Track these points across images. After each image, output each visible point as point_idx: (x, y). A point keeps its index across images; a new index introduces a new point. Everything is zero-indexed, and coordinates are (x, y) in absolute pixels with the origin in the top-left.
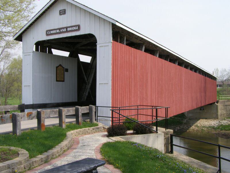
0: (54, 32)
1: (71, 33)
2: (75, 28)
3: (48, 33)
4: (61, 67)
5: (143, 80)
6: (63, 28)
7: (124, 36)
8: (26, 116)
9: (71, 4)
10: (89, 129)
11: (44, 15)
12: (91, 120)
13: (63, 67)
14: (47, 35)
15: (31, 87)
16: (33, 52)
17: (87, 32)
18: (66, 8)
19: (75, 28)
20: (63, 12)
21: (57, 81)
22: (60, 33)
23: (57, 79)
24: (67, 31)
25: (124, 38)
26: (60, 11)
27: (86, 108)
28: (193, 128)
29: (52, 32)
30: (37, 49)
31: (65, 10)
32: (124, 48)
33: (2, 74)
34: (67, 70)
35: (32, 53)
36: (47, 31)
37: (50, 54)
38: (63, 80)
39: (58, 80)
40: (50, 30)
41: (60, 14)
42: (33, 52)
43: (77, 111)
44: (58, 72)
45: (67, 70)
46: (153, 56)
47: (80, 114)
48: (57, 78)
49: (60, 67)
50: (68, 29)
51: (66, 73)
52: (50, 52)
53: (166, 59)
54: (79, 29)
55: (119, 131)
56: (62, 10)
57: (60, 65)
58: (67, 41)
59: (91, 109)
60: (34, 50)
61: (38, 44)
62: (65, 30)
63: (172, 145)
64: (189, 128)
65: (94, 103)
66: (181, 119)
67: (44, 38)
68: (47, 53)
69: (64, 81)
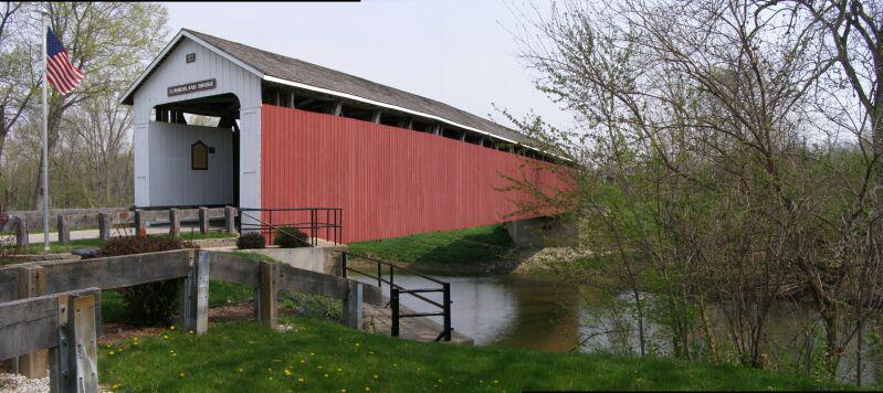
0: (179, 90)
2: (208, 84)
3: (171, 91)
12: (228, 230)
14: (170, 95)
20: (191, 59)
21: (193, 169)
22: (188, 92)
24: (198, 90)
28: (523, 267)
32: (291, 113)
34: (212, 150)
36: (169, 89)
37: (181, 125)
40: (173, 88)
41: (188, 62)
42: (150, 122)
43: (201, 214)
45: (212, 150)
51: (210, 155)
53: (395, 125)
54: (214, 86)
59: (227, 213)
60: (153, 118)
63: (345, 269)
64: (515, 267)
65: (236, 203)
67: (166, 100)
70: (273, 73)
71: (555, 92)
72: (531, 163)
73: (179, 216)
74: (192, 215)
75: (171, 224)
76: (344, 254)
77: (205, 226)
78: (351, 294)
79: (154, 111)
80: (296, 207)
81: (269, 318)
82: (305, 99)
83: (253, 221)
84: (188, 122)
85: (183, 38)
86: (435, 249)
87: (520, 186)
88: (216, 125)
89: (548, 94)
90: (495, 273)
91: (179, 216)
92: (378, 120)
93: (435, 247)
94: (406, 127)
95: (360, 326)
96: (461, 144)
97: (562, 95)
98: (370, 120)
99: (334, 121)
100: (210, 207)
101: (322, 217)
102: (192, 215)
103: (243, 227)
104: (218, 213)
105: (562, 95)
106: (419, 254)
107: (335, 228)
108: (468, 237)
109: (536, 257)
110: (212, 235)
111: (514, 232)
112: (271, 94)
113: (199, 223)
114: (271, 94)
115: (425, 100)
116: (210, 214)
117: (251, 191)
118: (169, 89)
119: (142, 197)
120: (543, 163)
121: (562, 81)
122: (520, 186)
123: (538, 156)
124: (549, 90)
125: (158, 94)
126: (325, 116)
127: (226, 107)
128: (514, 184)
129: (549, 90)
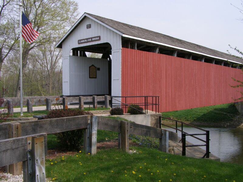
0: (83, 41)
1: (94, 42)
2: (97, 39)
3: (80, 42)
4: (93, 67)
5: (156, 76)
6: (89, 38)
7: (135, 43)
8: (55, 100)
9: (94, 21)
10: (100, 111)
11: (77, 28)
12: (106, 107)
13: (95, 67)
14: (79, 43)
15: (69, 82)
16: (70, 56)
17: (105, 42)
18: (91, 23)
19: (97, 39)
20: (89, 27)
21: (90, 78)
23: (95, 78)
24: (92, 41)
25: (135, 44)
26: (87, 25)
27: (102, 97)
29: (82, 41)
30: (74, 54)
31: (90, 25)
32: (135, 52)
33: (60, 71)
34: (99, 69)
35: (69, 58)
36: (79, 41)
37: (84, 58)
38: (95, 77)
39: (90, 77)
40: (81, 40)
41: (87, 28)
42: (70, 56)
43: (94, 99)
44: (91, 71)
45: (99, 69)
46: (171, 56)
47: (96, 101)
48: (90, 75)
49: (92, 67)
50: (93, 39)
51: (98, 71)
52: (85, 55)
53: (183, 57)
54: (100, 39)
55: (117, 112)
56: (88, 25)
57: (93, 65)
58: (96, 46)
59: (106, 98)
60: (71, 54)
61: (75, 51)
62: (90, 40)
65: (110, 94)
66: (233, 115)
67: (77, 46)
68: (79, 56)
69: (96, 78)
70: (127, 33)
73: (83, 99)
74: (90, 99)
75: (80, 104)
76: (160, 117)
77: (96, 105)
78: (163, 136)
79: (72, 51)
80: (138, 96)
81: (125, 147)
82: (142, 45)
83: (118, 102)
84: (88, 56)
85: (85, 17)
86: (203, 115)
88: (100, 57)
91: (83, 99)
92: (176, 55)
94: (189, 58)
95: (167, 151)
96: (213, 65)
98: (172, 55)
99: (156, 55)
100: (98, 95)
101: (150, 100)
102: (90, 99)
103: (113, 105)
104: (101, 99)
106: (195, 117)
107: (156, 106)
108: (216, 109)
110: (99, 109)
111: (239, 108)
112: (126, 43)
113: (93, 103)
114: (126, 43)
115: (197, 45)
116: (98, 99)
117: (117, 88)
118: (79, 41)
119: (66, 91)
125: (73, 43)
126: (151, 54)
127: (105, 49)
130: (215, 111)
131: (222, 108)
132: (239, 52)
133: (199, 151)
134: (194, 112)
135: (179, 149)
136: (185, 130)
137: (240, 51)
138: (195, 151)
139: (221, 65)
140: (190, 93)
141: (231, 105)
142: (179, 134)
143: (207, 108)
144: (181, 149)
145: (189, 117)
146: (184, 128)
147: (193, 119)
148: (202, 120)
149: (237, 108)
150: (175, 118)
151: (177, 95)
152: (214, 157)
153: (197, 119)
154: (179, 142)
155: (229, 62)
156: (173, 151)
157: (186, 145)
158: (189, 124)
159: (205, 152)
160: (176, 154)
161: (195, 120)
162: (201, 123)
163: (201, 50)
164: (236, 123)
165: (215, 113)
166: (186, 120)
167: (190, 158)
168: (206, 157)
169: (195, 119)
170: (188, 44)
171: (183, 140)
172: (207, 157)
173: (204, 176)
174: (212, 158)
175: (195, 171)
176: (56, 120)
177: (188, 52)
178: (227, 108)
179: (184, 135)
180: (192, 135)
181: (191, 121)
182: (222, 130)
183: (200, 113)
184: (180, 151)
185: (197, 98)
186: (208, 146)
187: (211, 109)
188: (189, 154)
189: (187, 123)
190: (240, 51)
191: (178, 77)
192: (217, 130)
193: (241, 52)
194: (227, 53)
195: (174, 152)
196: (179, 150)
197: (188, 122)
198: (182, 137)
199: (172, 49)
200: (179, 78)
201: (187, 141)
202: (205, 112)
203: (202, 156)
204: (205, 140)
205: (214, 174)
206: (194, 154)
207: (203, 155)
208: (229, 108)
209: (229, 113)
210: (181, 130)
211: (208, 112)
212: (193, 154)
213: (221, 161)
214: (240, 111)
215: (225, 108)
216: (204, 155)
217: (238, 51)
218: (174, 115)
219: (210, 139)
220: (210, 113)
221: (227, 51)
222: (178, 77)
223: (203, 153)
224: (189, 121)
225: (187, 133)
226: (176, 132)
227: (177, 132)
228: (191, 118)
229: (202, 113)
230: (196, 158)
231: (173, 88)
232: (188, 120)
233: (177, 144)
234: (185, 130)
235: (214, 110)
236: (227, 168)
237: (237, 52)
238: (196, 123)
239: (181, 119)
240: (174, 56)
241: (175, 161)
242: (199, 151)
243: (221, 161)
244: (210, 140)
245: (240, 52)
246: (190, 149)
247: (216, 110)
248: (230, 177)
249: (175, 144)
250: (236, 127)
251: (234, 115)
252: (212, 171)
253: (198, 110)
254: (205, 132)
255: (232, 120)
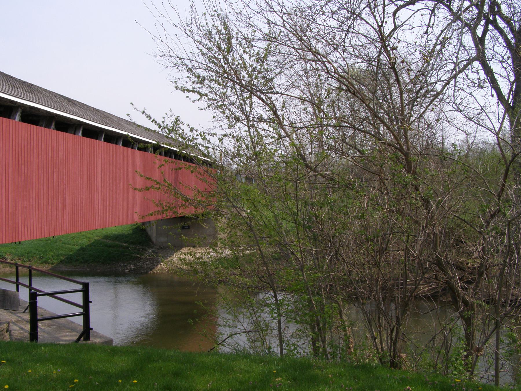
66: (143, 249)
71: (194, 91)
72: (169, 163)
86: (79, 250)
87: (159, 185)
89: (187, 93)
90: (134, 273)
92: (18, 117)
93: (78, 247)
94: (48, 126)
96: (100, 144)
97: (200, 94)
105: (200, 94)
106: (62, 255)
108: (107, 237)
109: (175, 257)
111: (153, 233)
120: (182, 163)
121: (201, 81)
122: (159, 185)
123: (177, 156)
124: (188, 90)
128: (153, 184)
129: (188, 90)
130: (104, 240)
131: (120, 235)
132: (150, 118)
133: (69, 328)
134: (61, 245)
135: (23, 326)
136: (39, 284)
137: (153, 118)
138: (61, 328)
139: (116, 144)
140: (50, 203)
141: (136, 228)
142: (24, 295)
143: (89, 235)
144: (28, 327)
145: (49, 255)
146: (34, 279)
147: (57, 259)
148: (77, 260)
149: (149, 233)
150: (17, 258)
151: (20, 208)
152: (101, 337)
153: (67, 259)
154: (24, 312)
155: (130, 139)
156: (7, 335)
157: (39, 317)
158: (50, 269)
159: (82, 329)
160: (16, 339)
161: (62, 261)
162: (75, 266)
163: (75, 110)
164: (147, 265)
165: (106, 246)
166: (42, 263)
167: (46, 345)
168: (82, 339)
169: (62, 258)
170: (48, 95)
171: (33, 307)
172: (85, 340)
173: (75, 381)
174: (98, 340)
175: (55, 372)
176: (6, 277)
177: (47, 112)
178: (129, 234)
179: (33, 296)
180: (51, 295)
181: (52, 264)
182: (121, 279)
183: (74, 245)
184: (26, 331)
185: (65, 213)
186: (86, 315)
187: (98, 236)
188: (46, 335)
189: (45, 268)
190: (153, 118)
191: (23, 167)
192: (110, 282)
193: (153, 120)
194: (127, 118)
195: (10, 335)
196: (22, 329)
197: (47, 265)
198: (30, 299)
199: (9, 104)
200: (26, 168)
201: (41, 308)
202: (85, 242)
203: (75, 338)
204: (81, 302)
205: (97, 373)
206: (58, 335)
207: (76, 335)
208: (133, 234)
209: (132, 243)
210: (28, 284)
211: (90, 243)
212: (56, 335)
213: (114, 344)
214: (154, 240)
215: (126, 233)
216: (78, 335)
217: (149, 117)
218: (13, 251)
219: (90, 300)
220: (94, 246)
221: (128, 115)
222: (23, 167)
223: (77, 332)
224: (49, 264)
225: (40, 291)
226: (16, 290)
227: (18, 290)
228: (53, 256)
229: (77, 246)
230: (59, 344)
231: (10, 191)
232: (46, 262)
233: (19, 317)
234: (39, 284)
235: (103, 239)
236: (123, 358)
237: (148, 119)
238: (63, 268)
239: (30, 261)
240: (15, 119)
241: (9, 356)
242: (69, 328)
243: (114, 344)
244: (91, 302)
245: (152, 120)
246: (50, 326)
247: (107, 239)
248: (127, 375)
249: (14, 318)
250: (147, 272)
251: (144, 247)
252: (93, 367)
253: (70, 239)
254: (80, 287)
255: (138, 259)
